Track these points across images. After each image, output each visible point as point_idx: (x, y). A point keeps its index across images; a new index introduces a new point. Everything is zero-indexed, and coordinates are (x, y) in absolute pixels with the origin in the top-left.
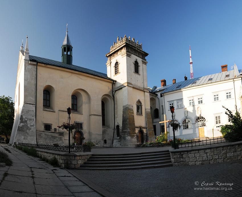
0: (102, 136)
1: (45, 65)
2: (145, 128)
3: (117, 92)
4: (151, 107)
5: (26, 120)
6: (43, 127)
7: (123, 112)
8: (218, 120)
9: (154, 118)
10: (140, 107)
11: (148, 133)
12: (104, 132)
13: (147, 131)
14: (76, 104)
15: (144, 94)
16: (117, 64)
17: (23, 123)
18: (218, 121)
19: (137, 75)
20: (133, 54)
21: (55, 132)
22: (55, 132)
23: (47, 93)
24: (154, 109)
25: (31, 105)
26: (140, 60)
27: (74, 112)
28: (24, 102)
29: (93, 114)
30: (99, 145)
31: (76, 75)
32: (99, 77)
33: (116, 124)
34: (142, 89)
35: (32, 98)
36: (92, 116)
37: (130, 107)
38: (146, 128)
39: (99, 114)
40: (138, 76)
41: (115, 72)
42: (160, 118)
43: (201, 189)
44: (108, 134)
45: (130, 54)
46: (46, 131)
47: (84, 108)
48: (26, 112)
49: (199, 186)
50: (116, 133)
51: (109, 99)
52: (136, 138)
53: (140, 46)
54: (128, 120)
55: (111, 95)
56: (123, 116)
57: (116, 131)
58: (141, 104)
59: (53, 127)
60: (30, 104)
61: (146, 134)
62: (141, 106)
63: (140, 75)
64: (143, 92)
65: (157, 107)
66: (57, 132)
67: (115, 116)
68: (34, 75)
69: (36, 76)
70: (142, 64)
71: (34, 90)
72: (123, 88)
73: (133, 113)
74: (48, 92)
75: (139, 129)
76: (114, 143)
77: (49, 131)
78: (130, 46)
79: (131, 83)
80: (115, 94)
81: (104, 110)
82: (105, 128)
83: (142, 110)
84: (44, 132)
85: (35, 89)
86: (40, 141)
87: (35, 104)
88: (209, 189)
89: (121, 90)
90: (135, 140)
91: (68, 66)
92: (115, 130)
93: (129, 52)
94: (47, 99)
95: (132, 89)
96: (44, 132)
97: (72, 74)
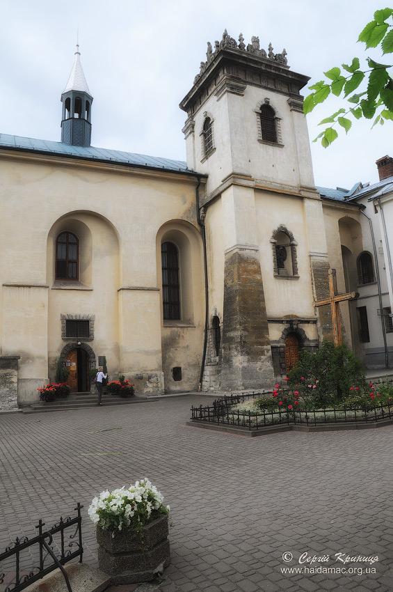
0: (161, 355)
2: (308, 322)
3: (210, 210)
4: (343, 247)
7: (226, 272)
10: (289, 249)
12: (168, 344)
13: (317, 330)
14: (75, 258)
16: (208, 123)
19: (270, 149)
20: (251, 84)
24: (358, 254)
26: (279, 102)
27: (65, 284)
29: (125, 285)
30: (149, 388)
33: (212, 313)
34: (296, 191)
36: (125, 292)
37: (246, 253)
40: (277, 150)
41: (206, 148)
43: (298, 570)
44: (187, 346)
49: (295, 563)
50: (211, 344)
51: (188, 236)
52: (273, 358)
53: (281, 59)
54: (245, 300)
55: (193, 221)
56: (225, 286)
57: (210, 337)
61: (314, 341)
62: (293, 246)
63: (282, 146)
65: (367, 245)
67: (207, 287)
72: (223, 195)
73: (258, 271)
76: (206, 378)
78: (240, 61)
80: (204, 217)
81: (178, 269)
82: (176, 329)
88: (319, 571)
90: (264, 365)
92: (209, 333)
93: (239, 79)
94: (64, 247)
95: (251, 193)
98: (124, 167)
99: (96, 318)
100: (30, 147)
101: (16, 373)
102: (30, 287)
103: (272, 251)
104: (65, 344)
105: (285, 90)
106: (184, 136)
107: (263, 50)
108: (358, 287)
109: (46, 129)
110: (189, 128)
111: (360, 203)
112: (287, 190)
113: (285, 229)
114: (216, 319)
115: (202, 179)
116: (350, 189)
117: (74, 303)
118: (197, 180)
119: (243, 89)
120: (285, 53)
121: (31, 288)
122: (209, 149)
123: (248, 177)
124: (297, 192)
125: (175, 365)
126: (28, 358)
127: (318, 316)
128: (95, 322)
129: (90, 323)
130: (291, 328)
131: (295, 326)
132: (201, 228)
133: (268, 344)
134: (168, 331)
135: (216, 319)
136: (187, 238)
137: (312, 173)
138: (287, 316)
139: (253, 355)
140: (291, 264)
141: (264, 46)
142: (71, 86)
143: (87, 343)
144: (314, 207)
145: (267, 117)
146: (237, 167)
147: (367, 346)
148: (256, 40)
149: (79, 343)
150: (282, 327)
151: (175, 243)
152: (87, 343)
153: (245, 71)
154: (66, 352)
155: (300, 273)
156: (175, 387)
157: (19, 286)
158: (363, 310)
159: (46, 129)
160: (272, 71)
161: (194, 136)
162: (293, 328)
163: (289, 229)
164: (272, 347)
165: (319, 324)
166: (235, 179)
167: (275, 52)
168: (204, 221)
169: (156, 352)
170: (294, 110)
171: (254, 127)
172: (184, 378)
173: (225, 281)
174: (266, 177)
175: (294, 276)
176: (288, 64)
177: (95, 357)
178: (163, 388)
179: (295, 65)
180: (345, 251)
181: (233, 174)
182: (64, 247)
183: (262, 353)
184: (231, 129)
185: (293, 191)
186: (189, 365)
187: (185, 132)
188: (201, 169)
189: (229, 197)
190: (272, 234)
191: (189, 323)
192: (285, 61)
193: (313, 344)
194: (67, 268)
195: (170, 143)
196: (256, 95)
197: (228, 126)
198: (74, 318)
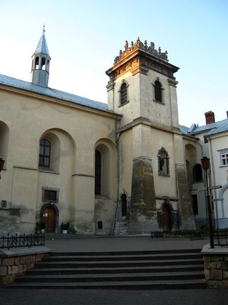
0: (93, 214)
2: (174, 200)
3: (123, 134)
4: (187, 161)
7: (133, 170)
11: (181, 211)
12: (98, 207)
13: (178, 205)
16: (124, 86)
19: (159, 105)
20: (151, 69)
21: (4, 208)
22: (4, 208)
26: (163, 79)
29: (77, 173)
33: (121, 192)
34: (170, 129)
44: (106, 210)
54: (142, 185)
55: (113, 140)
56: (133, 178)
61: (176, 211)
62: (167, 159)
66: (7, 208)
70: (168, 86)
80: (119, 138)
81: (101, 166)
82: (100, 200)
89: (129, 133)
95: (149, 129)
98: (81, 106)
99: (60, 190)
101: (18, 218)
104: (44, 203)
105: (166, 73)
106: (107, 90)
107: (156, 50)
110: (111, 86)
111: (196, 137)
112: (165, 129)
113: (164, 149)
114: (124, 196)
116: (189, 127)
117: (51, 181)
118: (117, 118)
119: (147, 71)
120: (166, 53)
121: (29, 170)
122: (124, 100)
123: (148, 120)
124: (170, 130)
125: (99, 220)
126: (26, 210)
127: (179, 197)
128: (60, 193)
129: (57, 192)
130: (166, 202)
131: (168, 202)
132: (117, 145)
134: (97, 200)
135: (124, 196)
136: (107, 147)
137: (178, 120)
138: (164, 197)
139: (149, 216)
140: (166, 168)
141: (156, 48)
142: (207, 111)
144: (178, 138)
145: (158, 86)
148: (153, 44)
150: (162, 202)
151: (101, 152)
153: (162, 68)
155: (170, 174)
156: (99, 233)
157: (22, 168)
158: (195, 197)
159: (24, 74)
161: (114, 91)
164: (158, 213)
165: (179, 201)
166: (141, 121)
167: (162, 52)
169: (91, 212)
172: (103, 228)
173: (133, 174)
175: (167, 175)
176: (168, 59)
179: (172, 60)
180: (187, 162)
181: (141, 118)
184: (141, 93)
186: (106, 220)
187: (108, 88)
188: (119, 111)
189: (138, 130)
190: (158, 152)
191: (107, 197)
192: (167, 57)
193: (175, 212)
195: (98, 92)
196: (153, 75)
197: (139, 91)
198: (49, 189)
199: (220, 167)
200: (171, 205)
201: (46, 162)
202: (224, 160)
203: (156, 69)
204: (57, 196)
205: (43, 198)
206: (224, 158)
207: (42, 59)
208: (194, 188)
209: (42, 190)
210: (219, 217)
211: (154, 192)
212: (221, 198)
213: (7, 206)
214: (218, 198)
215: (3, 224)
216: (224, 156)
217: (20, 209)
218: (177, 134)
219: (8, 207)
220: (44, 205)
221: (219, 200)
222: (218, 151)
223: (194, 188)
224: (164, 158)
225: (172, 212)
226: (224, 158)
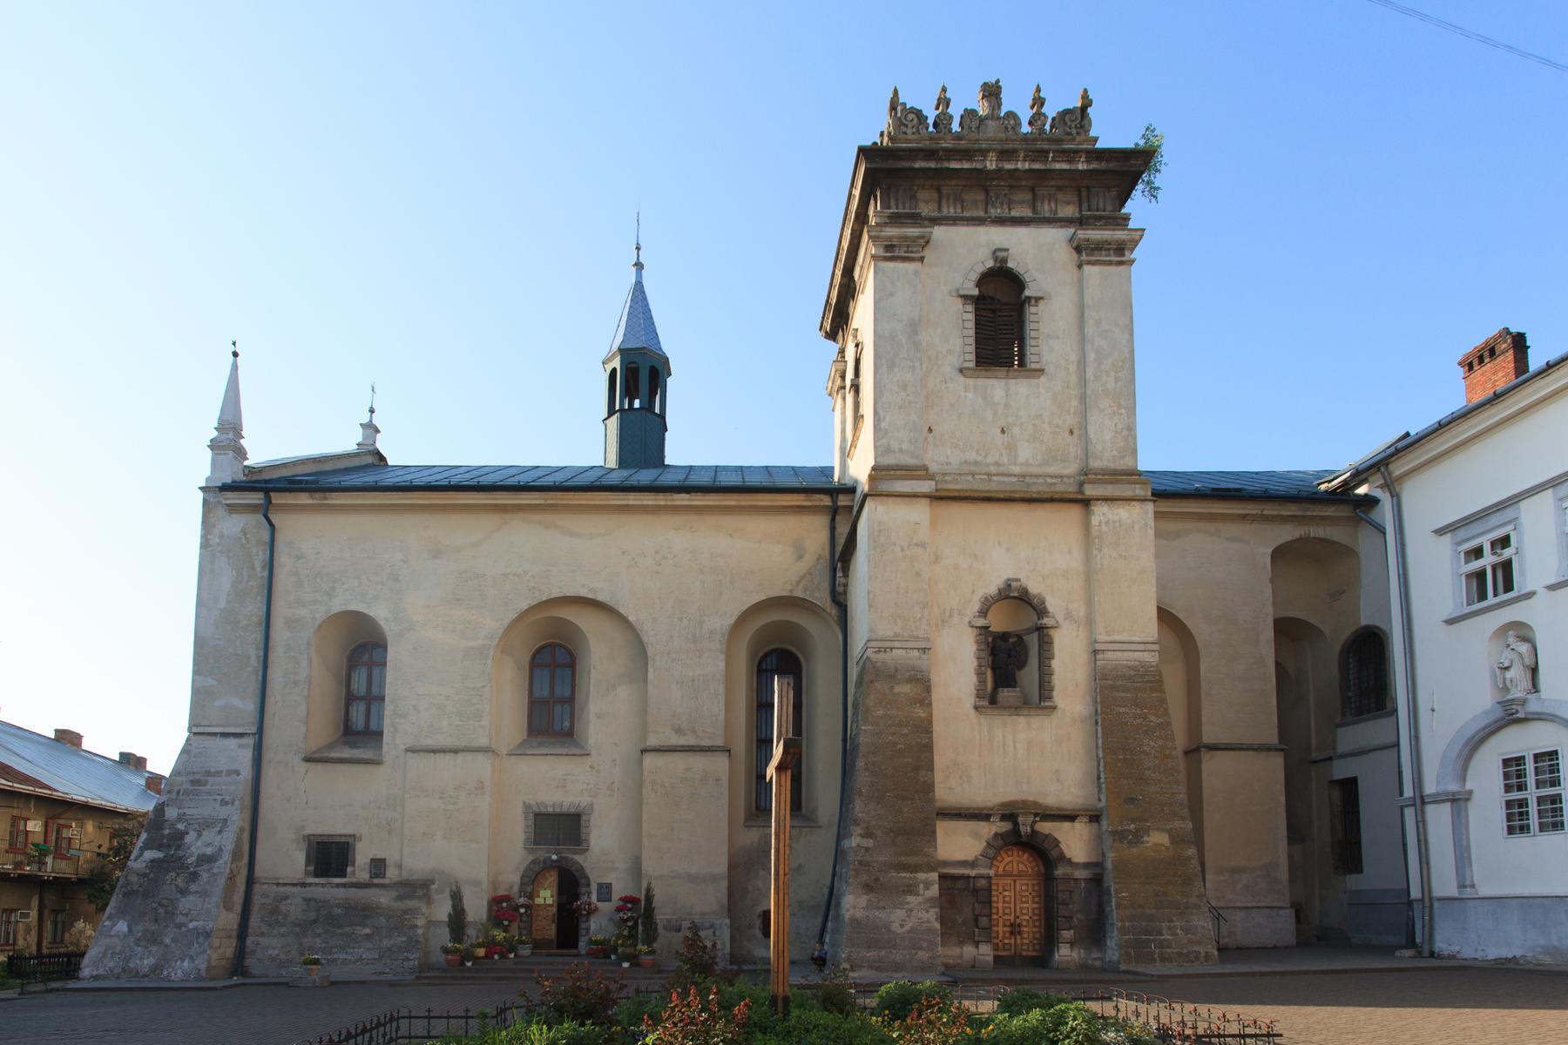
0: (724, 884)
1: (317, 495)
2: (1070, 817)
5: (181, 826)
6: (300, 858)
8: (1532, 794)
9: (1344, 714)
11: (1109, 864)
13: (1099, 838)
15: (1086, 525)
17: (159, 848)
18: (1531, 779)
20: (935, 221)
21: (376, 881)
22: (376, 881)
23: (365, 658)
24: (1345, 635)
25: (233, 742)
26: (1038, 250)
28: (190, 730)
31: (537, 517)
32: (661, 496)
34: (1069, 488)
35: (236, 702)
38: (1095, 818)
39: (706, 743)
42: (519, 752)
44: (800, 867)
45: (913, 231)
46: (317, 880)
47: (606, 707)
48: (193, 782)
55: (822, 597)
58: (1041, 611)
59: (363, 856)
60: (224, 735)
61: (1086, 866)
62: (1045, 643)
64: (1075, 512)
66: (386, 881)
68: (258, 569)
69: (266, 574)
71: (254, 654)
74: (361, 649)
75: (1005, 826)
77: (343, 880)
79: (912, 461)
80: (846, 585)
83: (1056, 664)
84: (303, 885)
85: (262, 645)
86: (264, 941)
87: (253, 729)
91: (645, 476)
94: (546, 672)
96: (303, 885)
97: (507, 516)
100: (1033, 506)
102: (455, 751)
103: (974, 647)
104: (531, 858)
105: (1069, 211)
108: (1339, 726)
109: (585, 440)
115: (841, 497)
121: (460, 755)
133: (933, 870)
141: (1017, 102)
143: (577, 858)
146: (888, 450)
147: (1353, 881)
149: (554, 857)
151: (801, 658)
152: (577, 858)
154: (532, 878)
155: (1058, 698)
160: (1020, 165)
162: (1022, 832)
163: (1034, 588)
164: (942, 877)
168: (845, 593)
170: (1089, 263)
171: (954, 333)
174: (976, 463)
177: (589, 885)
178: (727, 950)
180: (1288, 631)
182: (546, 672)
183: (911, 889)
185: (1060, 488)
194: (552, 714)
198: (550, 810)
199: (1451, 622)
200: (1057, 843)
201: (552, 714)
202: (1480, 575)
203: (994, 212)
204: (584, 830)
205: (527, 841)
206: (1476, 565)
207: (640, 378)
208: (1341, 749)
209: (526, 813)
210: (1438, 892)
211: (929, 787)
212: (1453, 787)
213: (388, 874)
214: (1430, 788)
215: (368, 931)
216: (1477, 553)
217: (433, 882)
218: (1106, 499)
219: (392, 874)
220: (535, 862)
221: (1438, 799)
222: (1440, 532)
223: (1341, 749)
224: (1029, 631)
225: (1060, 871)
226: (1476, 565)
